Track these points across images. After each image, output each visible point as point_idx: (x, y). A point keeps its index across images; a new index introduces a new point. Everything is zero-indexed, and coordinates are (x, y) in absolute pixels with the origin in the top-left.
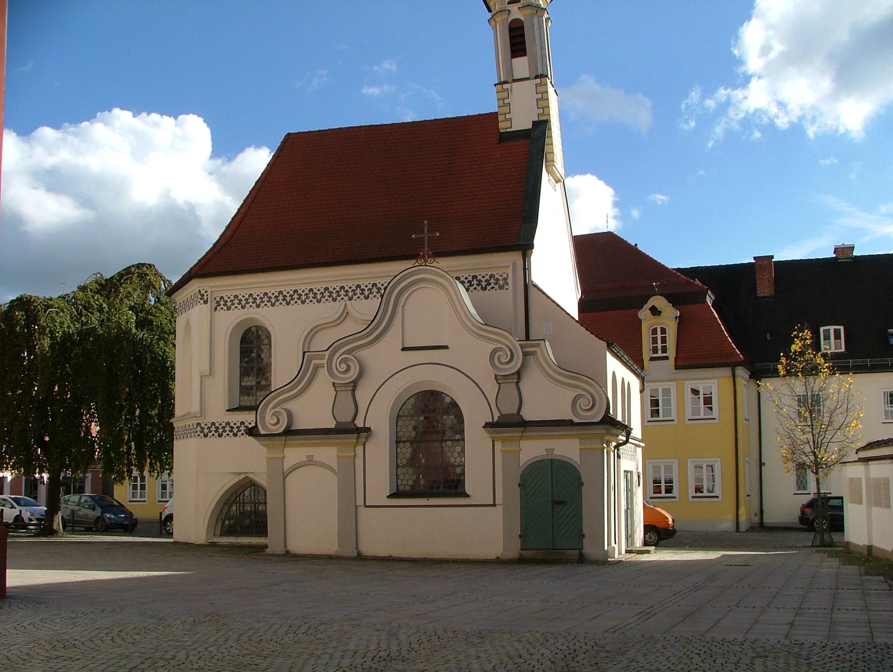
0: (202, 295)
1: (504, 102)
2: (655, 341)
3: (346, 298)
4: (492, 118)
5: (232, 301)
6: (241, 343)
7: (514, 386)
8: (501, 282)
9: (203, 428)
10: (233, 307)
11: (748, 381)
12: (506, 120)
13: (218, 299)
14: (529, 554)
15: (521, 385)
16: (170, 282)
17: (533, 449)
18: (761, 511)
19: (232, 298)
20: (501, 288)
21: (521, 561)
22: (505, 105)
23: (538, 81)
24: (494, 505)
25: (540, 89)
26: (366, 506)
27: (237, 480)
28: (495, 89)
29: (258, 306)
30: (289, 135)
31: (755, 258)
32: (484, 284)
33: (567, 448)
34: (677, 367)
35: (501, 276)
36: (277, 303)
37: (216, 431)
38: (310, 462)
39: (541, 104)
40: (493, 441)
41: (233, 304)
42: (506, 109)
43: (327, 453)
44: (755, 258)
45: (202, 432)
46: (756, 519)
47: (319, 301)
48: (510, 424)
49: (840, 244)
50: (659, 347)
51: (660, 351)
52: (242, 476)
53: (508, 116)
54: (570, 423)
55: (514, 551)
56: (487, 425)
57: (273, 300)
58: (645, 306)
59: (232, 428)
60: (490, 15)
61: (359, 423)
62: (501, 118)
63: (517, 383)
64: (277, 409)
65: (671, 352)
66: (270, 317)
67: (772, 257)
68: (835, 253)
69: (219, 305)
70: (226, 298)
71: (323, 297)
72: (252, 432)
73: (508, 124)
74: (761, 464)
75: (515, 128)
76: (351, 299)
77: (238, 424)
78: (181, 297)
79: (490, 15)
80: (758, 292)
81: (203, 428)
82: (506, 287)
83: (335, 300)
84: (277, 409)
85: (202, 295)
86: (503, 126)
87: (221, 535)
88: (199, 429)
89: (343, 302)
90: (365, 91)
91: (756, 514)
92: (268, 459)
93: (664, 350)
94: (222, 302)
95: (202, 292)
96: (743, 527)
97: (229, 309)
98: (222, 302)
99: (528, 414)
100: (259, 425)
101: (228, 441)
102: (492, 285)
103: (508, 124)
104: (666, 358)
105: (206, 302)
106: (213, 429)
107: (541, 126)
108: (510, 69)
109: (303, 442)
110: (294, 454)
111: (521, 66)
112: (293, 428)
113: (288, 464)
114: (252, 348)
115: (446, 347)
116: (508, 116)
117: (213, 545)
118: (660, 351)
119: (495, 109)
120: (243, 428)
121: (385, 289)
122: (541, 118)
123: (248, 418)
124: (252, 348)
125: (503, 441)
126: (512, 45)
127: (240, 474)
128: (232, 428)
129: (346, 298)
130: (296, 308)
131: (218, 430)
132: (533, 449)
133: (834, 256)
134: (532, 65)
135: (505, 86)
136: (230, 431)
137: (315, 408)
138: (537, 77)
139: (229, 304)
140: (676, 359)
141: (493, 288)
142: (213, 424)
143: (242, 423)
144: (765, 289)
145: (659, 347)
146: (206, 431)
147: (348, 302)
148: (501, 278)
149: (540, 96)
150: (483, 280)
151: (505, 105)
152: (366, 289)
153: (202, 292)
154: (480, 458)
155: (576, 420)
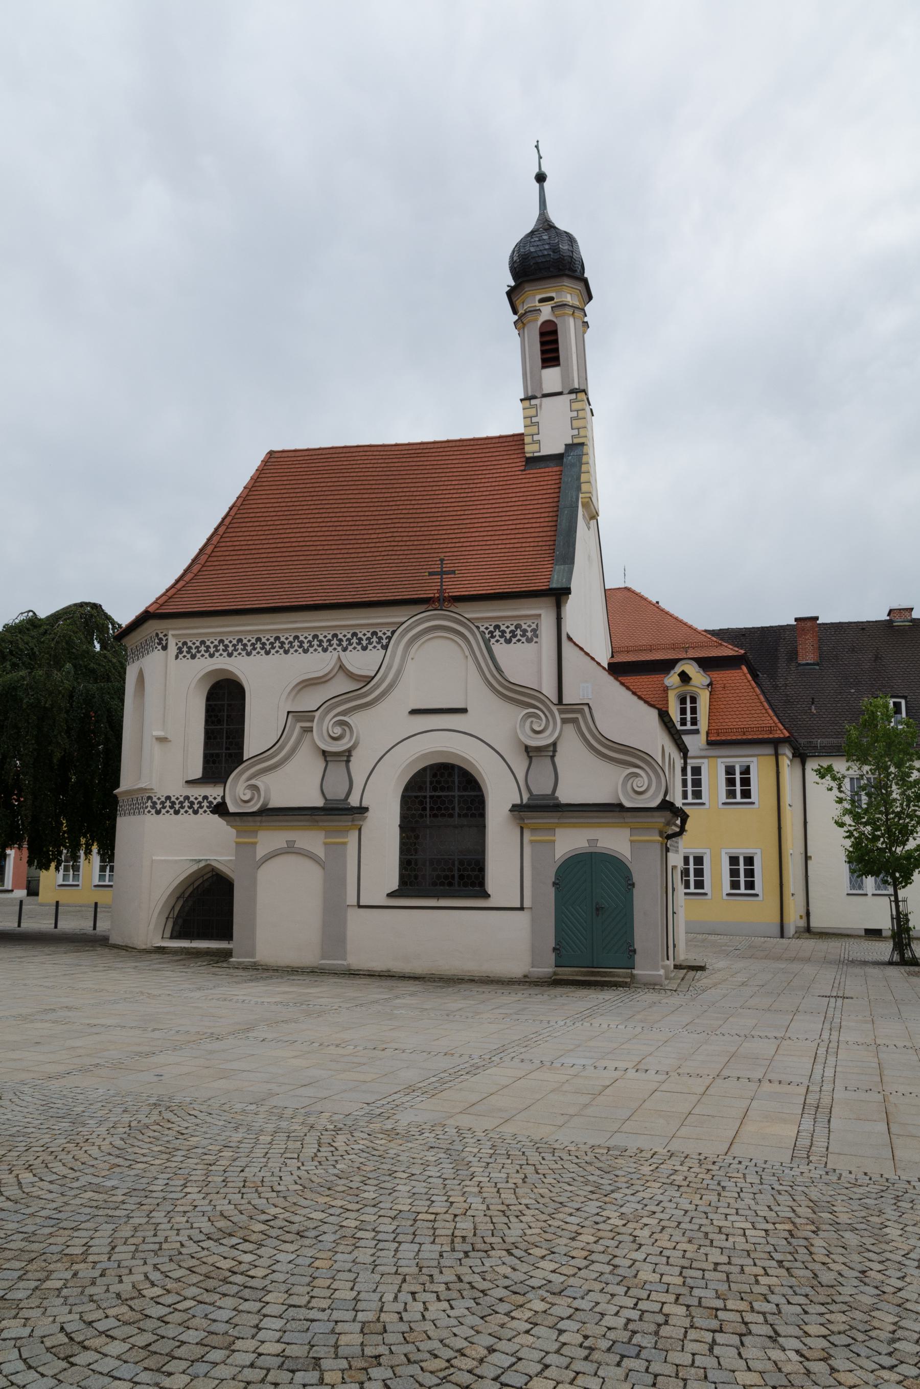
0: (161, 639)
1: (531, 421)
2: (694, 710)
3: (339, 649)
4: (517, 440)
5: (197, 647)
6: (208, 699)
7: (548, 760)
8: (529, 634)
9: (155, 803)
10: (198, 655)
11: (791, 761)
12: (534, 442)
13: (180, 645)
14: (566, 973)
15: (557, 759)
16: (120, 626)
17: (570, 841)
18: (808, 914)
19: (198, 644)
20: (529, 640)
21: (555, 982)
22: (533, 424)
23: (573, 396)
24: (522, 909)
25: (576, 406)
26: (360, 906)
27: (195, 867)
28: (520, 406)
29: (230, 655)
30: (271, 453)
31: (796, 620)
32: (508, 636)
33: (615, 840)
34: (710, 743)
35: (529, 626)
36: (311, 650)
37: (171, 807)
38: (290, 850)
39: (576, 423)
40: (522, 829)
41: (199, 652)
42: (534, 430)
43: (312, 840)
44: (796, 620)
45: (153, 807)
46: (802, 923)
47: (306, 651)
48: (539, 810)
49: (895, 605)
50: (689, 719)
51: (689, 723)
52: (202, 864)
53: (536, 438)
54: (619, 808)
55: (547, 969)
56: (515, 808)
57: (249, 648)
58: (672, 672)
59: (192, 803)
60: (516, 317)
61: (354, 801)
62: (527, 440)
63: (553, 757)
64: (253, 782)
65: (703, 725)
66: (243, 667)
67: (817, 618)
68: (889, 615)
69: (181, 652)
70: (190, 644)
71: (292, 647)
72: (220, 809)
73: (534, 447)
74: (807, 858)
75: (545, 452)
76: (345, 650)
77: (200, 799)
78: (131, 641)
79: (516, 317)
80: (800, 658)
81: (155, 803)
82: (535, 639)
83: (325, 650)
84: (253, 782)
85: (161, 639)
86: (530, 450)
87: (172, 937)
88: (149, 804)
89: (335, 654)
90: (11, 853)
91: (801, 917)
92: (238, 844)
93: (694, 722)
94: (185, 649)
95: (161, 636)
96: (791, 930)
97: (193, 657)
98: (185, 649)
99: (565, 795)
100: (228, 801)
101: (186, 819)
102: (519, 637)
103: (534, 447)
104: (697, 732)
105: (165, 648)
106: (168, 804)
107: (576, 451)
108: (539, 382)
109: (278, 824)
110: (269, 839)
111: (551, 378)
112: (270, 806)
113: (261, 852)
114: (225, 705)
115: (464, 711)
116: (536, 438)
117: (161, 950)
118: (689, 723)
119: (520, 429)
120: (205, 804)
121: (390, 638)
122: (576, 441)
123: (214, 793)
124: (225, 705)
125: (534, 830)
126: (556, 341)
127: (200, 861)
128: (192, 803)
129: (339, 649)
130: (276, 659)
131: (174, 806)
132: (570, 841)
133: (888, 618)
134: (566, 377)
135: (533, 402)
136: (189, 808)
137: (297, 783)
138: (571, 392)
139: (194, 651)
140: (708, 733)
141: (519, 640)
142: (168, 798)
143: (205, 798)
144: (808, 655)
145: (689, 719)
146: (159, 806)
147: (342, 654)
148: (529, 629)
150: (508, 631)
151: (533, 424)
152: (364, 638)
153: (161, 636)
154: (505, 853)
155: (627, 804)
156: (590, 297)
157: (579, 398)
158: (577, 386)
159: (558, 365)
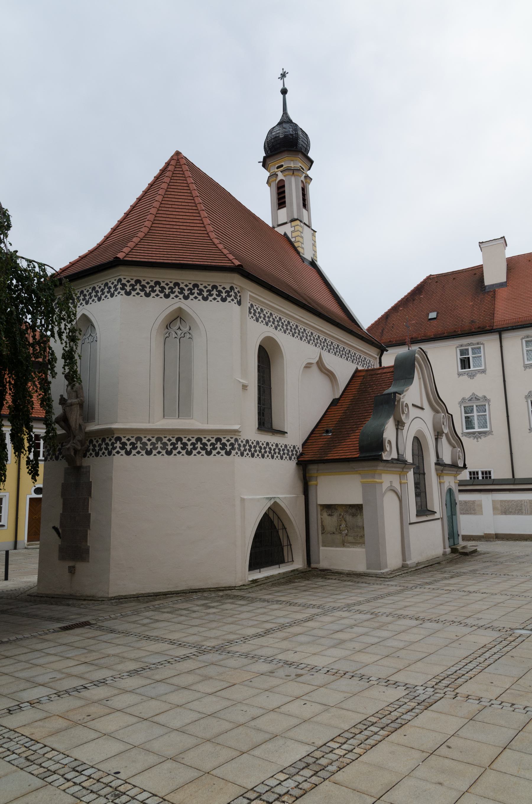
35: (167, 284)
134: (290, 212)
149: (293, 229)
156: (312, 162)
157: (296, 230)
158: (296, 217)
159: (285, 206)
